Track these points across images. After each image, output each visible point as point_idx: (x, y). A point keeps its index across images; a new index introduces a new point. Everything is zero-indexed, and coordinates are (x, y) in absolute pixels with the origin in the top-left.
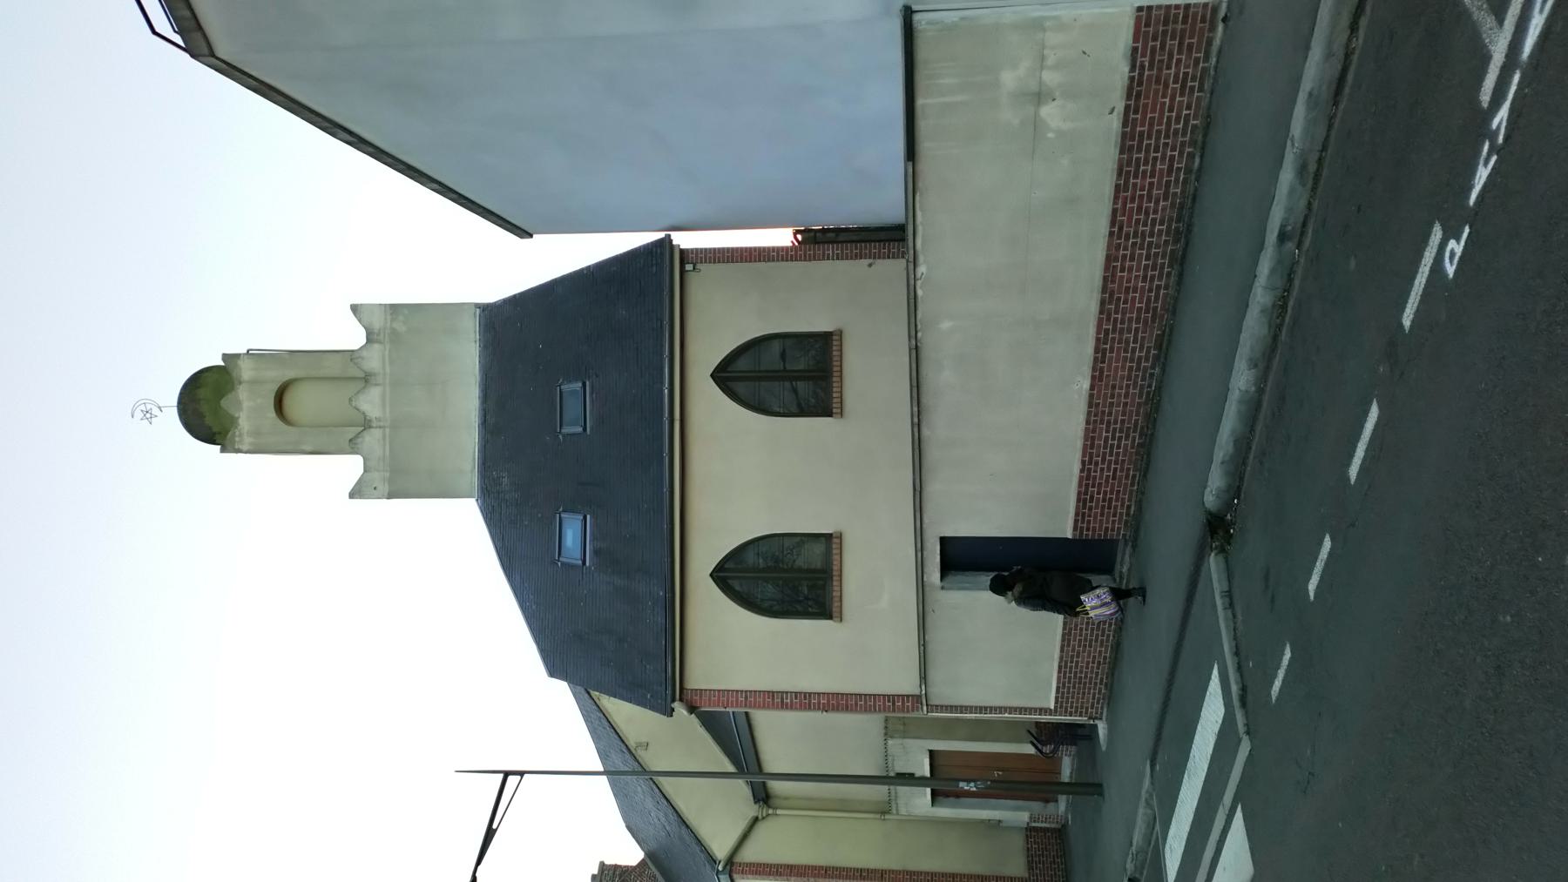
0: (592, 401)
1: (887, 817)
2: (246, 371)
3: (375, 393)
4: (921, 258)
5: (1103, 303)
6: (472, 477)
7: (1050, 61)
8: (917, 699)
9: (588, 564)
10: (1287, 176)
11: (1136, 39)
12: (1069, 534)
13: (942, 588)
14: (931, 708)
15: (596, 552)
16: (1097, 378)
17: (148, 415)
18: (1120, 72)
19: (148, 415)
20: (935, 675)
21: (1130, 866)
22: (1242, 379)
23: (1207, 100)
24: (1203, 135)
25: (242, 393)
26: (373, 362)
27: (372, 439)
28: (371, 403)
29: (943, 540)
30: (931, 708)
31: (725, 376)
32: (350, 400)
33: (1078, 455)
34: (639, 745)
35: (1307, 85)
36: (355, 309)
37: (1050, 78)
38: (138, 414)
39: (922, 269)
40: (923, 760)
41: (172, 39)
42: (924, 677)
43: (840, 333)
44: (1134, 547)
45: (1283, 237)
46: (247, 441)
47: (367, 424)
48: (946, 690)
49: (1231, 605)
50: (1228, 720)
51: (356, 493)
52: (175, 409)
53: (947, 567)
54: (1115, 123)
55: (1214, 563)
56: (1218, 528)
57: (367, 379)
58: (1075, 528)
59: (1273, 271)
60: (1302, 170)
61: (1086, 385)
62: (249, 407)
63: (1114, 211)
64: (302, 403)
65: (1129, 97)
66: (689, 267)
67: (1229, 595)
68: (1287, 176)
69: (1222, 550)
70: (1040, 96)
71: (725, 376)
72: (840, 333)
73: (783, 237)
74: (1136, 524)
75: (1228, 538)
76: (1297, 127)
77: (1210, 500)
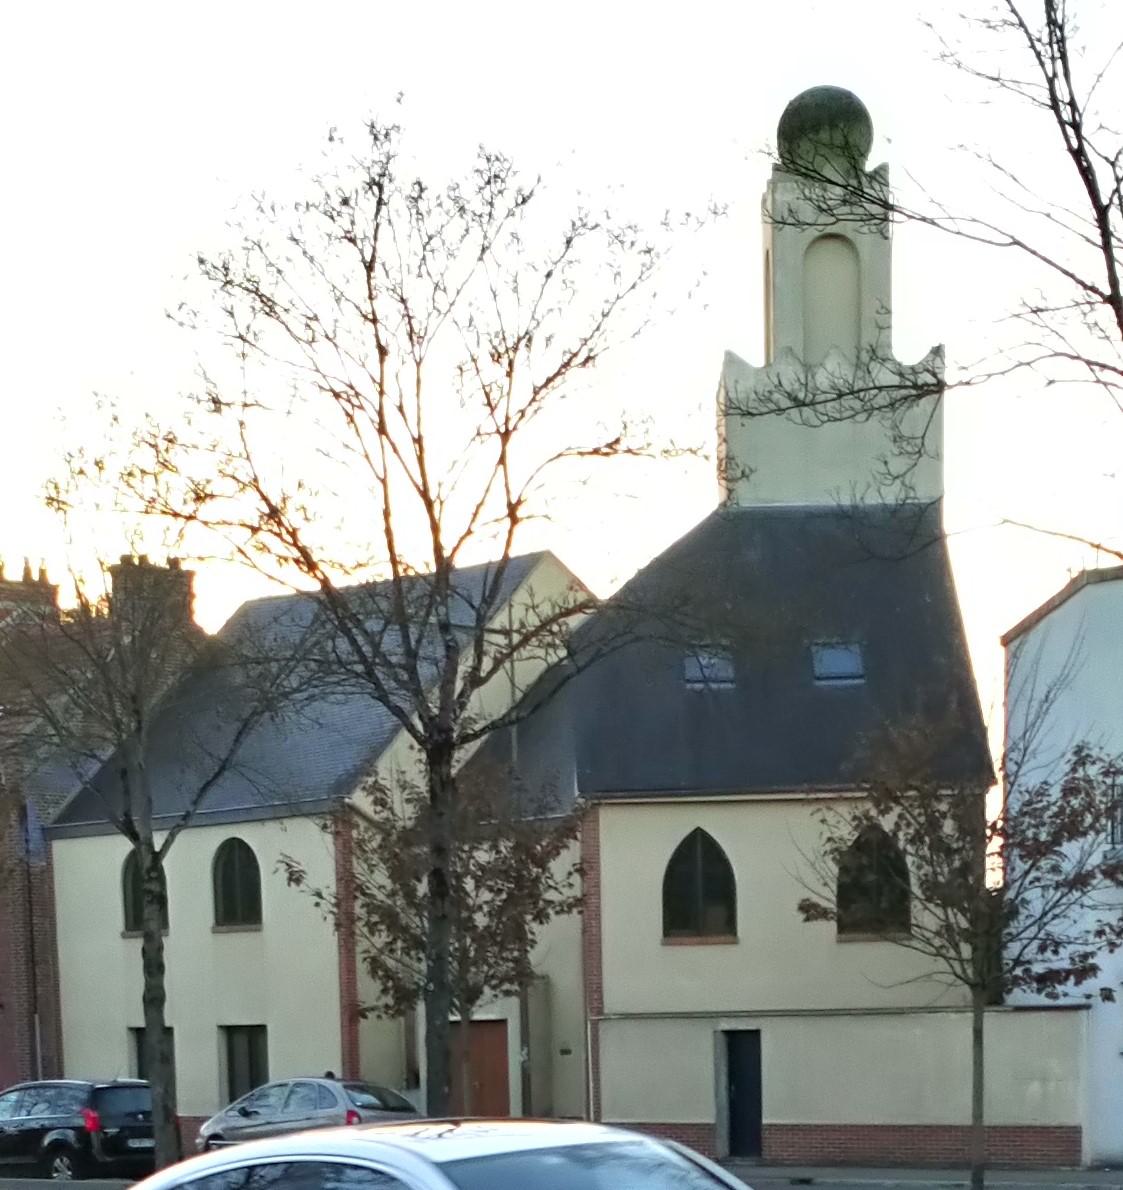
0: (846, 688)
1: (1077, 1168)
4: (958, 1016)
7: (1060, 1083)
8: (600, 1011)
9: (689, 686)
12: (765, 1121)
13: (715, 1032)
14: (595, 1024)
20: (630, 1027)
23: (510, 957)
29: (756, 1033)
32: (837, 347)
37: (1052, 1085)
39: (953, 1016)
40: (492, 1013)
41: (970, 1085)
48: (609, 1035)
53: (731, 1035)
58: (771, 1125)
70: (1044, 1080)
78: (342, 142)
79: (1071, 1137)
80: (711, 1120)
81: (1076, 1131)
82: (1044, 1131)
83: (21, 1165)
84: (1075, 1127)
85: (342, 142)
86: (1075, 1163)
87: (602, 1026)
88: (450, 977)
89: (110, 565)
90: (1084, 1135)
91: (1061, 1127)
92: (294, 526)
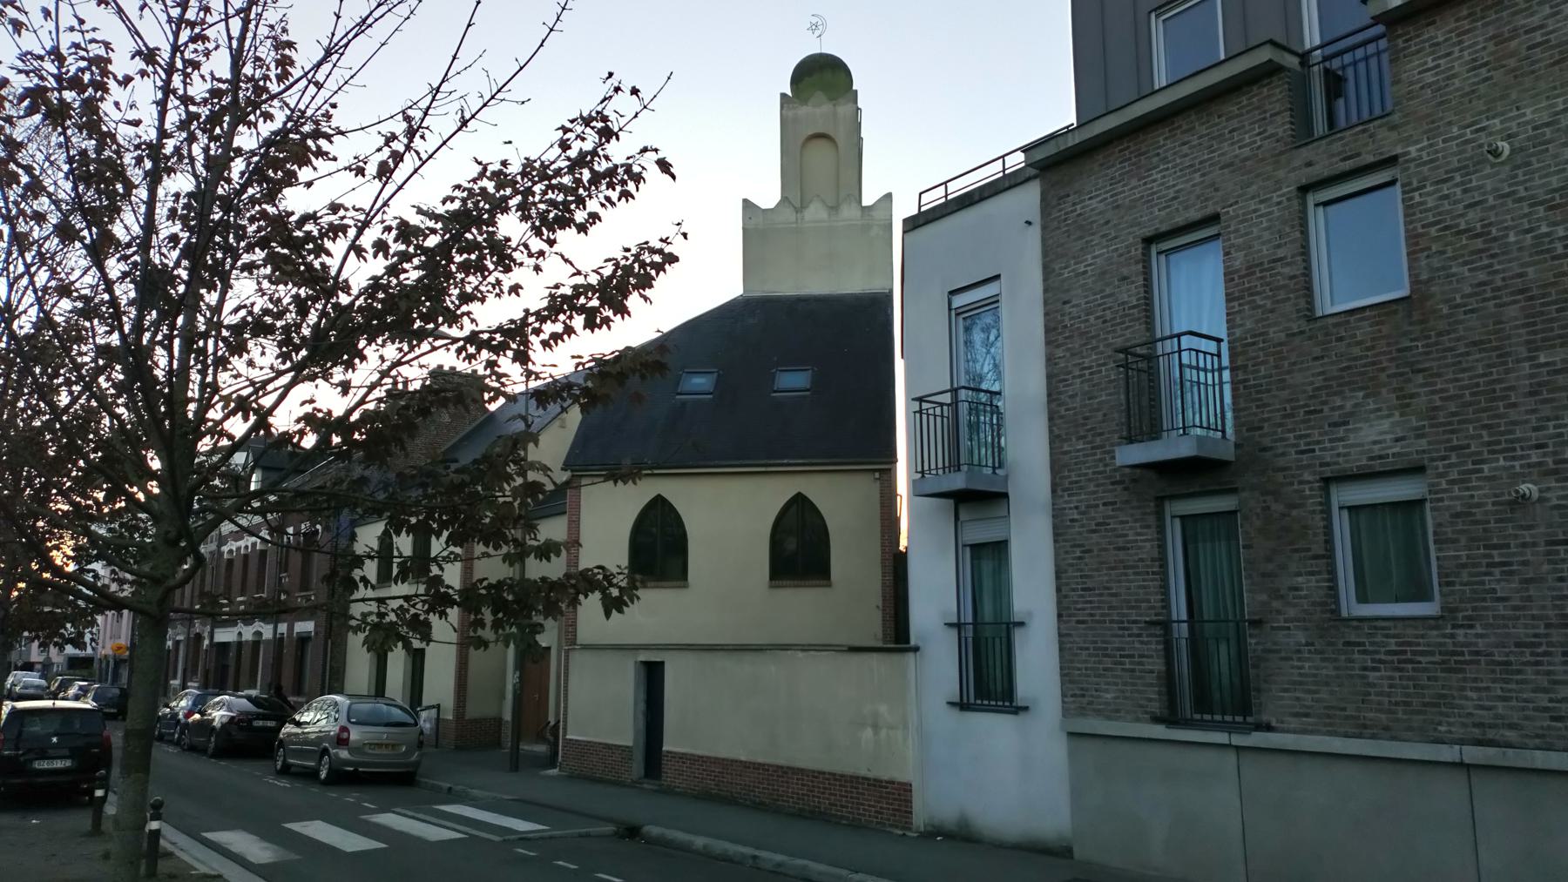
2: (844, 109)
3: (823, 214)
4: (805, 654)
5: (782, 767)
6: (757, 293)
10: (779, 858)
11: (899, 783)
14: (567, 652)
15: (684, 403)
16: (746, 765)
17: (814, 27)
18: (885, 775)
19: (814, 27)
21: (460, 787)
22: (700, 842)
24: (856, 826)
25: (826, 108)
26: (848, 212)
27: (789, 215)
28: (816, 212)
29: (662, 663)
30: (567, 652)
31: (799, 503)
33: (706, 753)
34: (563, 421)
35: (763, 854)
36: (889, 197)
37: (883, 733)
38: (814, 20)
39: (800, 654)
42: (586, 647)
43: (829, 585)
44: (656, 791)
45: (755, 857)
46: (790, 114)
47: (800, 209)
49: (581, 836)
50: (517, 832)
51: (748, 205)
52: (818, 51)
54: (863, 772)
55: (609, 828)
56: (631, 832)
57: (834, 209)
59: (742, 854)
60: (780, 865)
61: (743, 758)
62: (817, 113)
63: (824, 773)
64: (820, 150)
65: (875, 780)
66: (877, 475)
67: (588, 835)
68: (779, 858)
69: (616, 833)
71: (799, 503)
72: (829, 585)
73: (903, 543)
74: (669, 792)
75: (622, 837)
76: (799, 862)
77: (646, 829)
78: (686, 238)
79: (901, 793)
80: (630, 744)
81: (906, 788)
82: (876, 783)
83: (731, 841)
84: (905, 784)
85: (686, 238)
86: (907, 826)
87: (571, 654)
88: (150, 455)
89: (561, 465)
90: (914, 793)
91: (893, 782)
92: (151, 46)
